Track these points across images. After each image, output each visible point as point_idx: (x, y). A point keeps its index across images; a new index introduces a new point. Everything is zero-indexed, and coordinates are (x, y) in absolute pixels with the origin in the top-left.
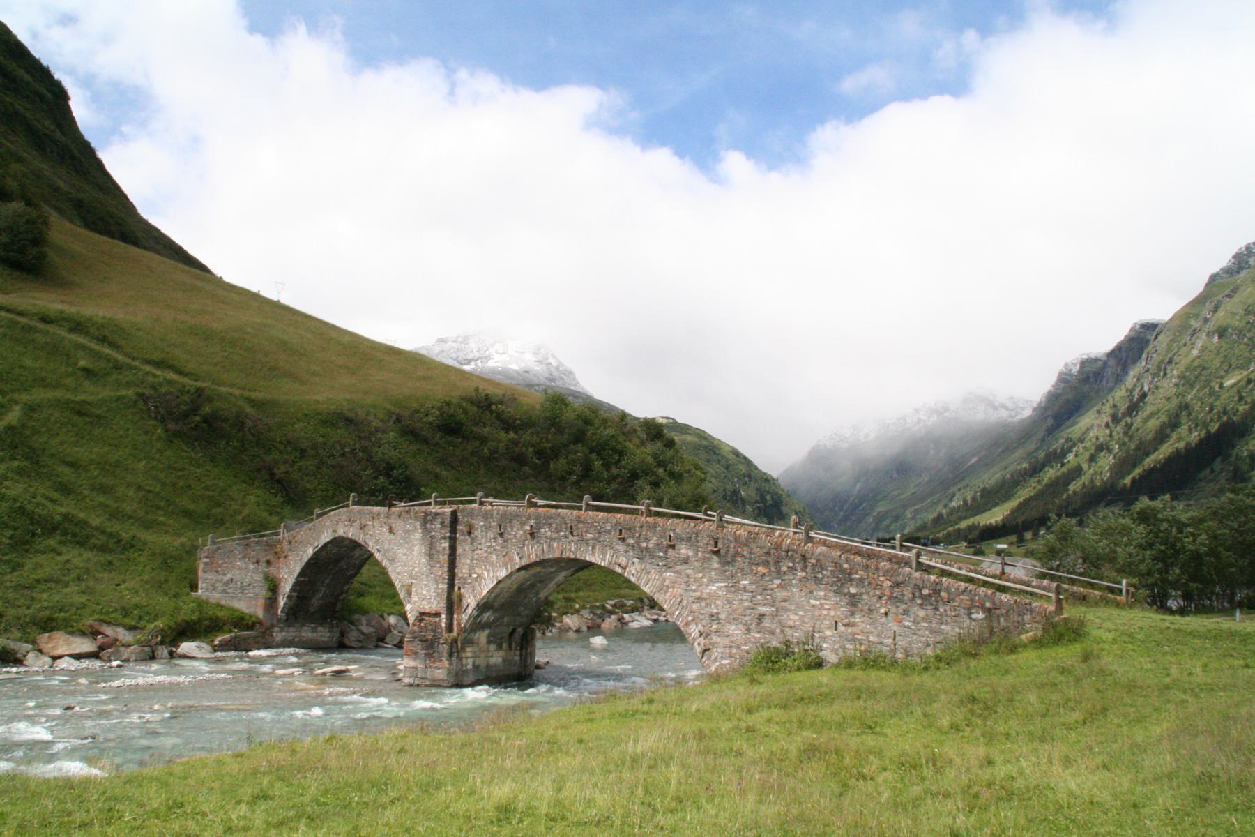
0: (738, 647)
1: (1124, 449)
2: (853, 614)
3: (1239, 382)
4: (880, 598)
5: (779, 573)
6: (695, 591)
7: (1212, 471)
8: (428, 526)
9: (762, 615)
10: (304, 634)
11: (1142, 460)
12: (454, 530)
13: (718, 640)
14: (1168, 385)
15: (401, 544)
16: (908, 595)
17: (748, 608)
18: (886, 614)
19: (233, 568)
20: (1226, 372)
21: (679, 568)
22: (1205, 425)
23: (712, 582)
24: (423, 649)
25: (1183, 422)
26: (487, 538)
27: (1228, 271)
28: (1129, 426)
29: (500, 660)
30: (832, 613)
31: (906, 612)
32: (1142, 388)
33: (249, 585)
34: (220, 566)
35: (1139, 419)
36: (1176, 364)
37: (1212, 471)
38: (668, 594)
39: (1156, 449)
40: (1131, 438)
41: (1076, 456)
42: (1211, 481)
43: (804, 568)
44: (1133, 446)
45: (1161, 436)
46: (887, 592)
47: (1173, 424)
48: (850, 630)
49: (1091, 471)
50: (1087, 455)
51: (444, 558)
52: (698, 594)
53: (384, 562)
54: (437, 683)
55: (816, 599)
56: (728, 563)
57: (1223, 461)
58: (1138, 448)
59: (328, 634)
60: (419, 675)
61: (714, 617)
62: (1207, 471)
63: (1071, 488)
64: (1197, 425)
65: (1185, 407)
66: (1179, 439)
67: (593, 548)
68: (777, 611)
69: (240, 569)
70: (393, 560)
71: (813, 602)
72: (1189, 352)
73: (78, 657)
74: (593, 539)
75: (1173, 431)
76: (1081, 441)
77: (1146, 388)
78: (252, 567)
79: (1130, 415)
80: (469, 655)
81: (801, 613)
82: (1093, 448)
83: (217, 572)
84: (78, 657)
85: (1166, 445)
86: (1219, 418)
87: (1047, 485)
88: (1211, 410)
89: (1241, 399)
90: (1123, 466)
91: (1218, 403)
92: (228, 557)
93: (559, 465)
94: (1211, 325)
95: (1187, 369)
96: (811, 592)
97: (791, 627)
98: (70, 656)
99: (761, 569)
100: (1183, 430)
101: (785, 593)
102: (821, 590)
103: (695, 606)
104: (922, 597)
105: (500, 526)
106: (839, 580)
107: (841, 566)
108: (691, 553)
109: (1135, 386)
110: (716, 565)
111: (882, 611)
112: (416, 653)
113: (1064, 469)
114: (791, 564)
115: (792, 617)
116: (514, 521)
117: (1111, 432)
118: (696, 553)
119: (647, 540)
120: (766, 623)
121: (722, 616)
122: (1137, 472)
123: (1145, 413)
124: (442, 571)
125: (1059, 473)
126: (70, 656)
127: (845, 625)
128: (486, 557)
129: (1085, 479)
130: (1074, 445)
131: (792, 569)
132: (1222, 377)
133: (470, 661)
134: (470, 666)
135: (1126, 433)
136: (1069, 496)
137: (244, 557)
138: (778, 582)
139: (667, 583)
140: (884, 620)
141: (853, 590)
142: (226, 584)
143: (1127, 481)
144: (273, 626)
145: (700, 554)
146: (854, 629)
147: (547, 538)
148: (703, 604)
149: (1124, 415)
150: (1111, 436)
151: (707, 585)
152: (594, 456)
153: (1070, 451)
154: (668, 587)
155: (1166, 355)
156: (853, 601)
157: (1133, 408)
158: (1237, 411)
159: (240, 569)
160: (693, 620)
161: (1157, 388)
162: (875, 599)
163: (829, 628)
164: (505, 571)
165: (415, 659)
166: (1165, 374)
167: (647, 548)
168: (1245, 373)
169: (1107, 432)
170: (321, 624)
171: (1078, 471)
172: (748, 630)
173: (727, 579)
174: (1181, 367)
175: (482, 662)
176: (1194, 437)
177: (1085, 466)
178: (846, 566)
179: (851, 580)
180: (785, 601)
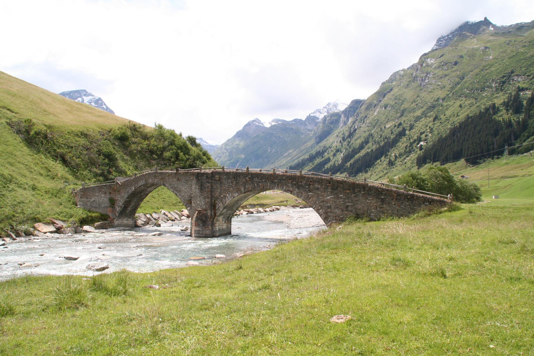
0: (339, 216)
1: (347, 151)
2: (382, 204)
3: (391, 126)
4: (393, 199)
5: (354, 193)
7: (381, 161)
8: (200, 178)
10: (124, 222)
11: (354, 156)
13: (331, 214)
15: (183, 185)
16: (403, 198)
17: (342, 204)
18: (395, 204)
19: (95, 196)
20: (387, 122)
22: (379, 143)
24: (202, 223)
27: (388, 81)
28: (349, 142)
29: (225, 227)
30: (375, 204)
31: (402, 203)
32: (355, 127)
34: (89, 195)
35: (353, 140)
36: (368, 118)
37: (381, 161)
38: (310, 200)
39: (359, 152)
40: (350, 147)
41: (328, 154)
42: (380, 165)
43: (364, 191)
44: (351, 150)
45: (361, 147)
46: (395, 198)
47: (366, 142)
48: (381, 209)
49: (334, 160)
50: (332, 153)
52: (323, 200)
54: (207, 236)
56: (335, 189)
57: (385, 157)
58: (352, 151)
59: (132, 222)
60: (200, 233)
61: (329, 207)
62: (379, 161)
63: (326, 166)
64: (375, 143)
65: (371, 135)
66: (368, 148)
67: (278, 185)
69: (98, 196)
71: (367, 201)
72: (373, 114)
73: (51, 232)
75: (366, 145)
76: (330, 148)
77: (356, 127)
78: (103, 195)
79: (350, 138)
80: (217, 225)
82: (335, 150)
84: (51, 232)
85: (363, 150)
86: (384, 140)
87: (316, 165)
88: (381, 137)
89: (392, 133)
90: (347, 158)
92: (92, 192)
93: (167, 154)
96: (367, 198)
97: (359, 209)
98: (49, 232)
99: (348, 191)
100: (370, 144)
101: (356, 199)
103: (321, 204)
104: (408, 199)
106: (378, 194)
111: (393, 203)
112: (199, 225)
113: (323, 159)
117: (342, 144)
118: (322, 187)
119: (301, 182)
120: (350, 208)
121: (332, 207)
122: (352, 161)
125: (321, 160)
126: (49, 232)
129: (331, 163)
130: (327, 149)
131: (359, 191)
132: (385, 124)
133: (218, 227)
134: (218, 229)
135: (348, 145)
136: (325, 169)
137: (100, 191)
138: (354, 195)
139: (310, 196)
140: (394, 206)
141: (382, 197)
142: (92, 202)
143: (348, 164)
144: (114, 219)
146: (383, 209)
147: (256, 182)
148: (325, 203)
149: (347, 138)
150: (342, 146)
151: (326, 197)
152: (179, 151)
153: (326, 152)
154: (310, 198)
156: (383, 201)
157: (351, 135)
159: (98, 196)
161: (360, 127)
163: (374, 209)
165: (199, 227)
166: (364, 122)
167: (301, 185)
168: (394, 123)
169: (341, 144)
170: (129, 218)
171: (329, 160)
172: (343, 211)
174: (370, 119)
175: (221, 227)
176: (374, 147)
177: (332, 158)
179: (382, 194)
180: (357, 201)
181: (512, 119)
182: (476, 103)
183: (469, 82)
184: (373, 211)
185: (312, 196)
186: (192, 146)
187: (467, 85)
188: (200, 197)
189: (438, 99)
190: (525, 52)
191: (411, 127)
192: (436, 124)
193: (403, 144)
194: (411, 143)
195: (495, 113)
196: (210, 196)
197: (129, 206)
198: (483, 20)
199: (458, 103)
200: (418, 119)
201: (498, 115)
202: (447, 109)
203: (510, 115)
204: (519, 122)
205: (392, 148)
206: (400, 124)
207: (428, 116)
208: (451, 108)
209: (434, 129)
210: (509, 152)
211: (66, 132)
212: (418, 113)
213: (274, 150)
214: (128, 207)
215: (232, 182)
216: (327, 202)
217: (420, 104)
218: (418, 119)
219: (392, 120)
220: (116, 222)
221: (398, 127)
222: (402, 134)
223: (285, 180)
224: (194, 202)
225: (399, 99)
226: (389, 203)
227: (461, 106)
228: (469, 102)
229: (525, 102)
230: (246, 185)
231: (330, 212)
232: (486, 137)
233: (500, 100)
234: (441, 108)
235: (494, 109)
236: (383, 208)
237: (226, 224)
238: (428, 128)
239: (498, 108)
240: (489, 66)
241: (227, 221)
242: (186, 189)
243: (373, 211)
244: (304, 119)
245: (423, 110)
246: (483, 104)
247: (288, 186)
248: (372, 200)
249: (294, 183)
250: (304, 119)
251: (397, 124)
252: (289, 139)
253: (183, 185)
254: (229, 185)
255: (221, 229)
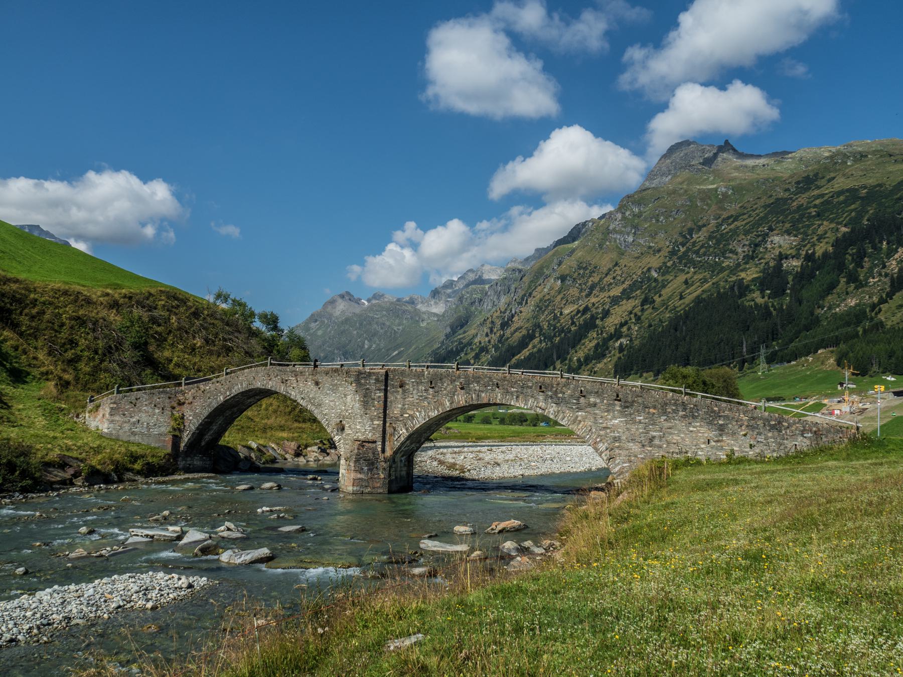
3: (572, 312)
5: (665, 413)
6: (602, 423)
8: (363, 381)
9: (654, 437)
10: (195, 463)
12: (386, 385)
14: (527, 310)
15: (327, 394)
17: (643, 433)
18: (745, 435)
20: (565, 304)
21: (588, 409)
23: (614, 418)
25: (537, 335)
26: (418, 390)
30: (706, 435)
32: (511, 311)
33: (155, 425)
36: (534, 297)
38: (581, 425)
39: (519, 353)
41: (466, 354)
43: (685, 409)
44: (504, 349)
50: (473, 354)
51: (379, 404)
52: (604, 425)
53: (309, 407)
55: (694, 427)
58: (508, 350)
61: (616, 439)
68: (664, 434)
70: (319, 405)
72: (542, 290)
74: (517, 392)
81: (682, 435)
83: (124, 415)
89: (573, 323)
91: (558, 325)
94: (557, 274)
95: (541, 300)
99: (652, 410)
100: (536, 341)
102: (697, 422)
103: (602, 433)
105: (431, 382)
107: (712, 408)
108: (598, 401)
109: (506, 310)
110: (618, 408)
114: (674, 408)
115: (675, 438)
116: (444, 380)
120: (657, 442)
123: (512, 329)
124: (376, 410)
127: (715, 442)
128: (417, 403)
130: (464, 347)
132: (562, 308)
138: (665, 417)
139: (579, 418)
141: (721, 422)
145: (605, 401)
148: (608, 431)
151: (611, 420)
154: (580, 421)
155: (527, 291)
156: (721, 429)
158: (571, 330)
160: (600, 441)
162: (736, 427)
163: (704, 443)
164: (436, 412)
166: (526, 303)
168: (576, 307)
172: (643, 446)
173: (626, 416)
178: (716, 409)
180: (670, 428)
181: (770, 304)
182: (711, 278)
183: (701, 243)
184: (703, 446)
185: (584, 419)
187: (695, 248)
188: (361, 416)
189: (649, 269)
190: (791, 198)
191: (606, 314)
192: (647, 309)
193: (589, 344)
194: (604, 339)
195: (742, 295)
196: (381, 415)
197: (208, 432)
198: (723, 144)
199: (682, 278)
200: (615, 301)
201: (747, 298)
202: (664, 286)
203: (766, 298)
204: (780, 310)
205: (574, 347)
206: (586, 309)
207: (633, 297)
208: (670, 285)
209: (642, 318)
210: (766, 358)
212: (616, 291)
213: (374, 346)
214: (205, 435)
215: (426, 390)
216: (613, 429)
217: (619, 278)
218: (615, 301)
219: (573, 303)
221: (583, 315)
222: (590, 325)
223: (531, 388)
224: (349, 427)
225: (585, 269)
226: (734, 434)
227: (686, 282)
228: (700, 276)
229: (790, 278)
230: (454, 395)
231: (618, 447)
233: (750, 274)
234: (654, 284)
235: (743, 289)
236: (722, 441)
238: (632, 316)
239: (748, 286)
240: (732, 220)
242: (332, 401)
243: (703, 446)
245: (625, 286)
246: (724, 281)
247: (536, 399)
248: (701, 426)
249: (550, 393)
251: (581, 309)
252: (401, 328)
253: (327, 394)
254: (421, 396)
255: (399, 476)
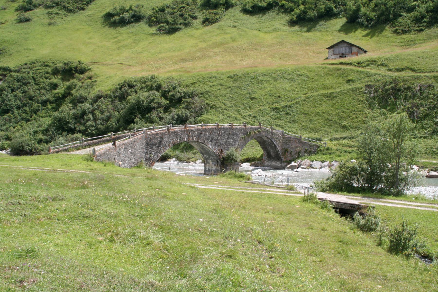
29: (215, 169)
133: (208, 168)
134: (208, 169)
144: (265, 160)
170: (278, 161)
186: (70, 81)
211: (225, 77)
220: (266, 163)
232: (189, 15)
237: (215, 167)
241: (216, 165)
244: (347, 20)
250: (347, 20)
